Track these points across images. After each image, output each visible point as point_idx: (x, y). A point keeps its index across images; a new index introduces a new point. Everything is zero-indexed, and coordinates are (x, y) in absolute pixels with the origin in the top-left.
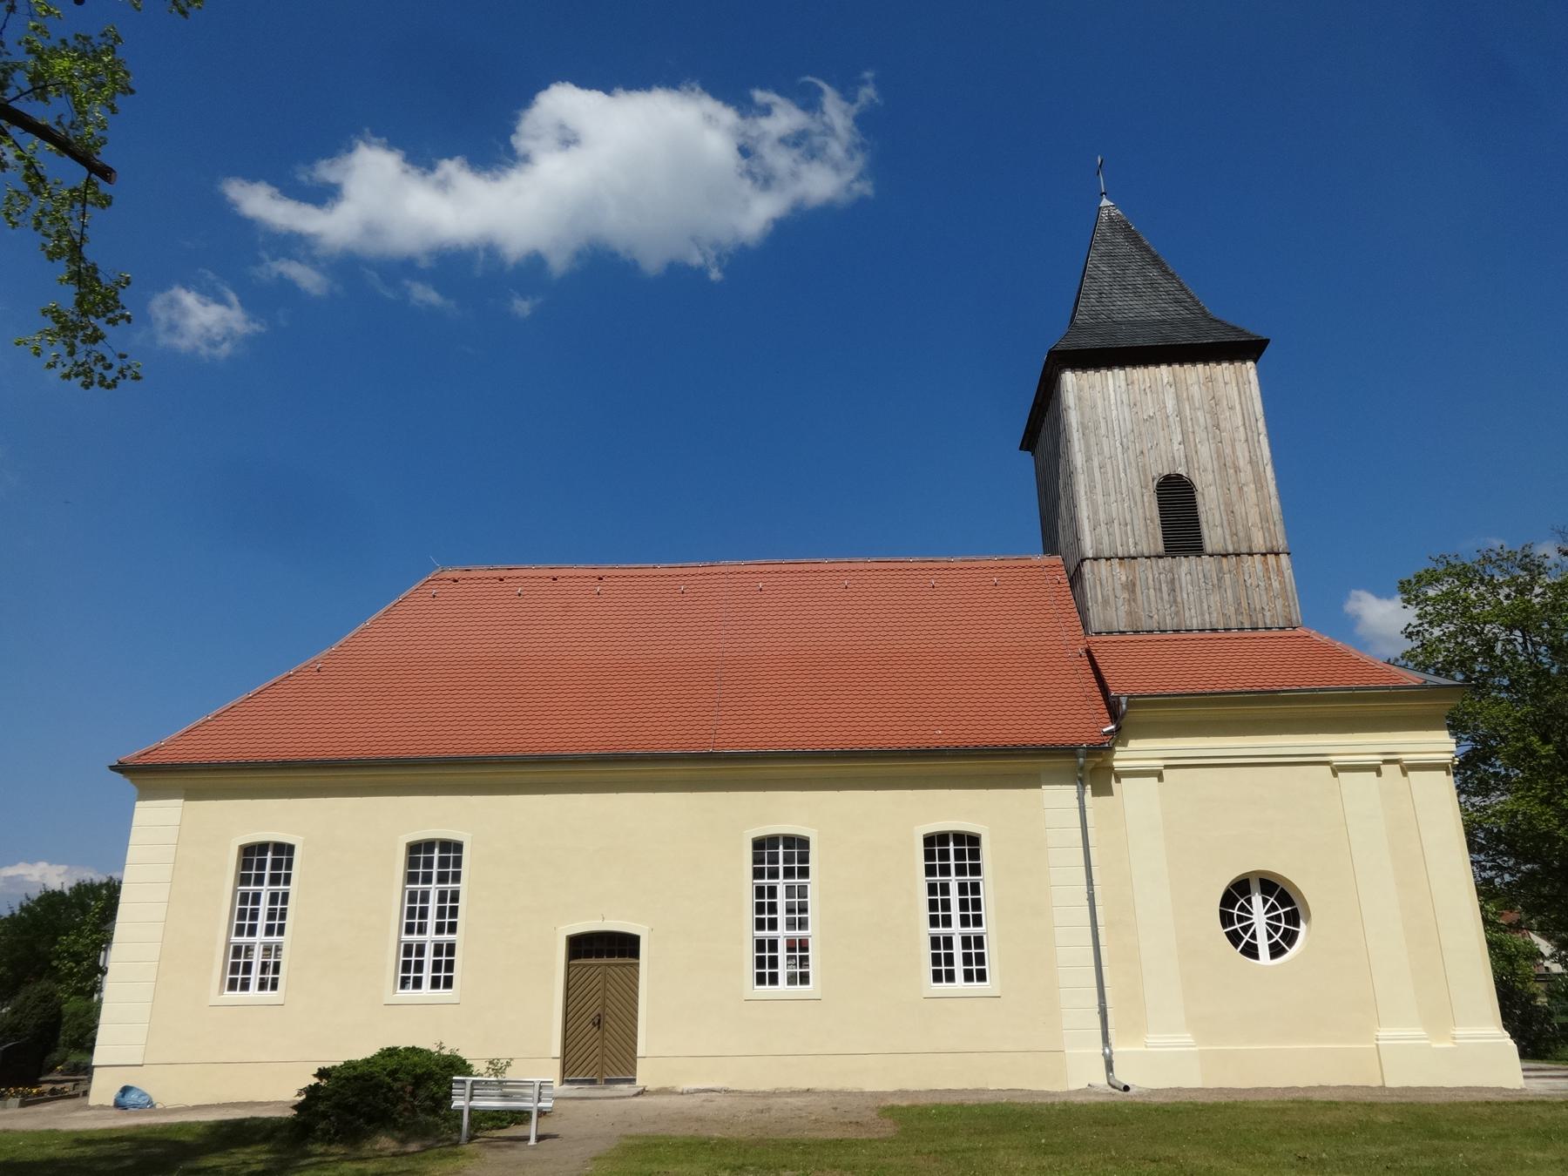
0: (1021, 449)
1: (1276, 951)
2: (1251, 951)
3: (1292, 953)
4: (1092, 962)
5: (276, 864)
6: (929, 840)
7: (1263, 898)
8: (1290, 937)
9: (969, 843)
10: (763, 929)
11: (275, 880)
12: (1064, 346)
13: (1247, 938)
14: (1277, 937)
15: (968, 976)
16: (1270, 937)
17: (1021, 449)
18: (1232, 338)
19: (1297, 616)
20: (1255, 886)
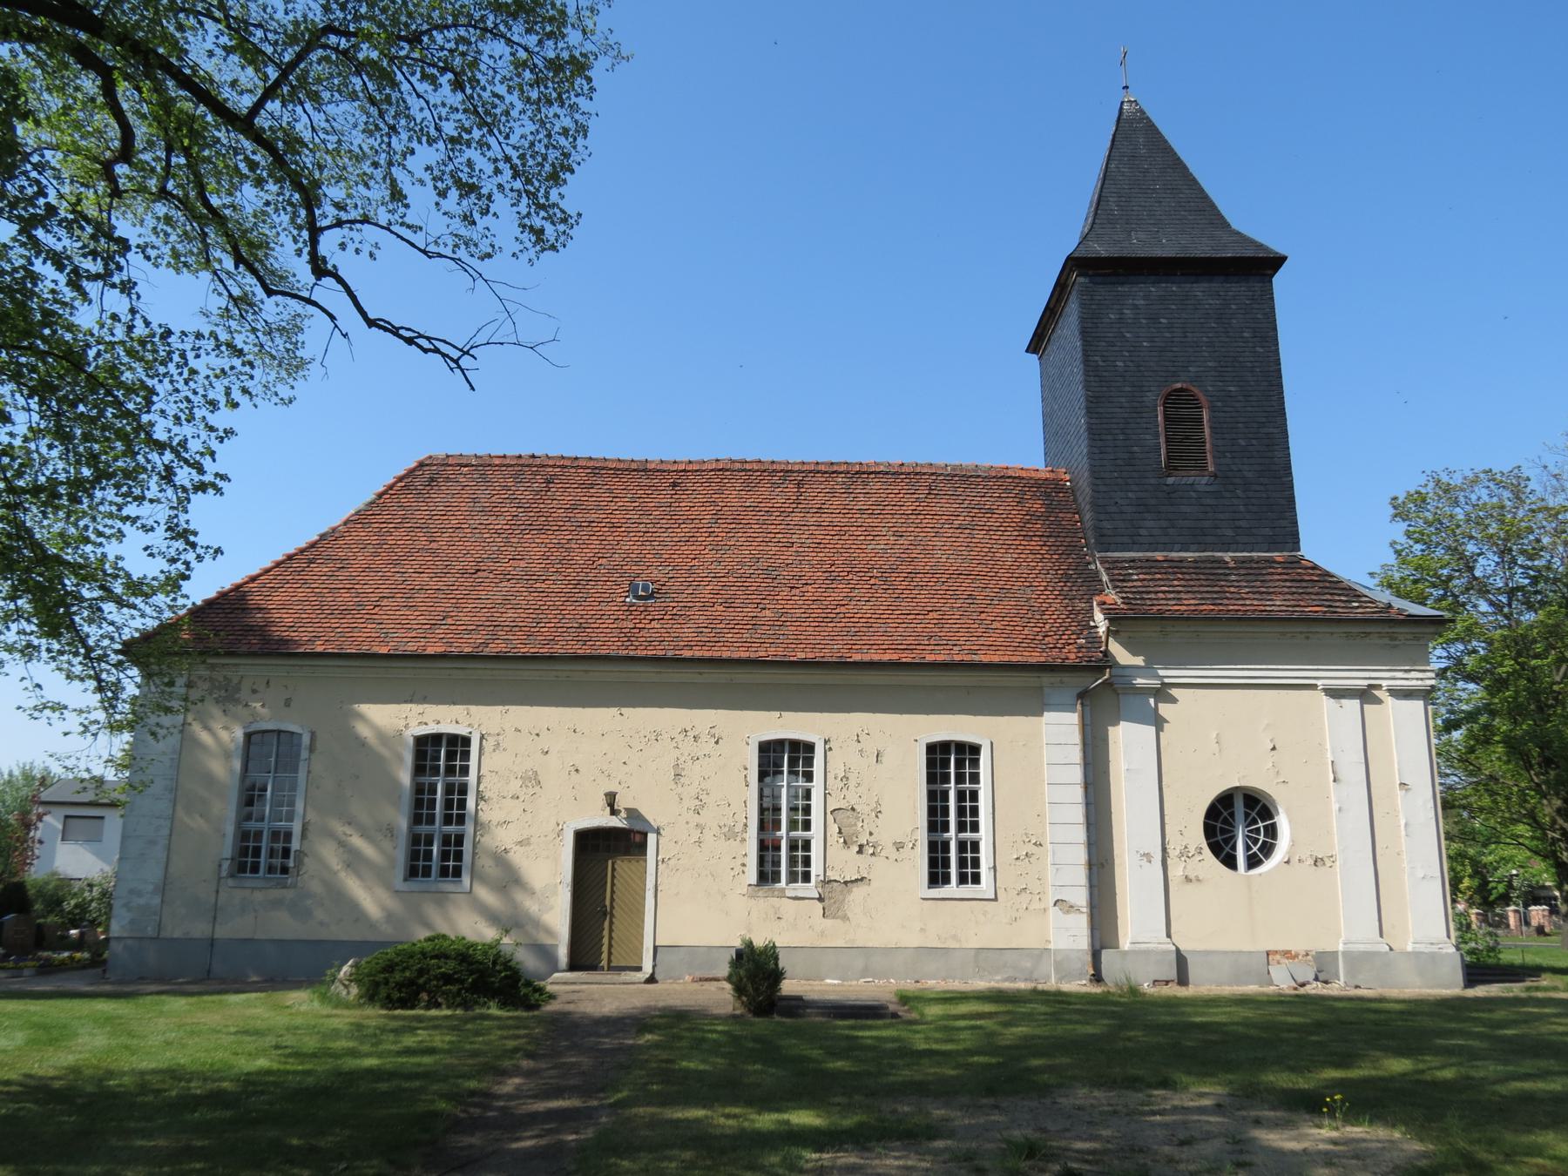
0: (1027, 351)
1: (1253, 862)
2: (1230, 862)
3: (1268, 866)
4: (1376, 830)
5: (451, 756)
6: (931, 748)
7: (1245, 813)
8: (1268, 849)
9: (969, 752)
10: (451, 824)
11: (450, 770)
12: (1082, 253)
13: (1227, 849)
14: (1255, 849)
15: (963, 879)
16: (1248, 848)
17: (1027, 351)
18: (1249, 253)
19: (1546, 989)
20: (1239, 807)
